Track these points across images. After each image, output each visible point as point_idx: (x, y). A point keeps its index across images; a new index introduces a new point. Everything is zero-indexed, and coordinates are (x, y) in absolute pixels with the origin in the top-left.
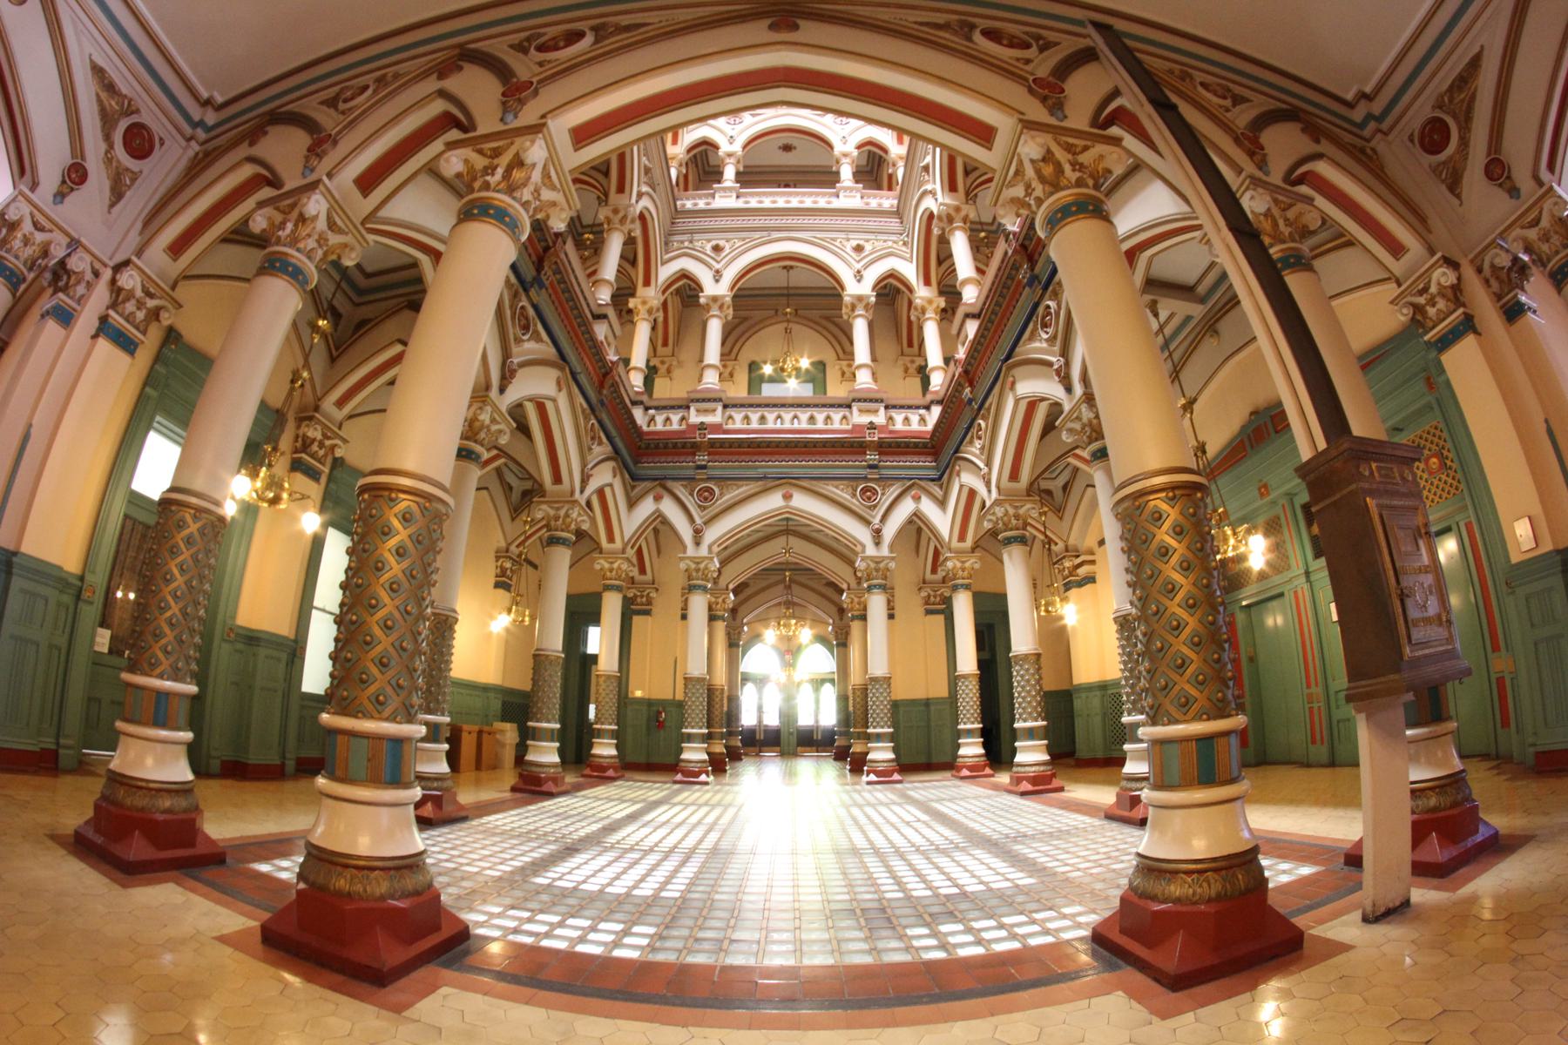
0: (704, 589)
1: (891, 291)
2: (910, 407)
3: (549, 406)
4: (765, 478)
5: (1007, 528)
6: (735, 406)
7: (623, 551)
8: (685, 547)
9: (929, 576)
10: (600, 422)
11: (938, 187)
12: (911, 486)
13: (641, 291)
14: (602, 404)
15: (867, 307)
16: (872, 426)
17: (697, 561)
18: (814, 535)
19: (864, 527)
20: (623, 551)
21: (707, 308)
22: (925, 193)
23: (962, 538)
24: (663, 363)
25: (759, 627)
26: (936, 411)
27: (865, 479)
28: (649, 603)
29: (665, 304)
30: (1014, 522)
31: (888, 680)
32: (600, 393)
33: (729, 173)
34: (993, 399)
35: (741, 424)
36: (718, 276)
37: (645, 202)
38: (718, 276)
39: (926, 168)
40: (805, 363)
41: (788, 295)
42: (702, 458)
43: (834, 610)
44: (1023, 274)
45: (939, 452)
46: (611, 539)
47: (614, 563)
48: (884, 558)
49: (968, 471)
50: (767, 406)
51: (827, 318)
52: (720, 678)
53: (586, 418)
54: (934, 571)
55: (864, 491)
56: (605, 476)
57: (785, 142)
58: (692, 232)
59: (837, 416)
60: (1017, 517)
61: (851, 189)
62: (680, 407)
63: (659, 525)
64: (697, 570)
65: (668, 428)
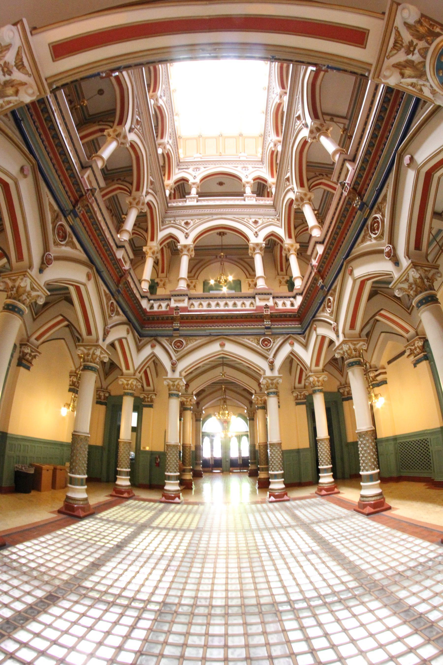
0: (178, 396)
1: (272, 245)
2: (285, 297)
3: (82, 288)
4: (210, 335)
5: (350, 357)
6: (194, 298)
7: (134, 374)
8: (167, 373)
9: (297, 385)
10: (118, 302)
11: (295, 185)
12: (289, 337)
13: (149, 243)
14: (118, 291)
15: (261, 249)
16: (267, 307)
17: (173, 380)
18: (237, 366)
19: (264, 361)
20: (134, 374)
21: (182, 250)
22: (288, 191)
23: (317, 364)
24: (161, 281)
25: (211, 411)
26: (299, 300)
27: (264, 335)
28: (152, 401)
29: (162, 249)
30: (354, 353)
31: (280, 444)
32: (118, 286)
33: (194, 191)
34: (338, 282)
35: (199, 307)
36: (187, 236)
37: (149, 198)
38: (187, 236)
39: (288, 179)
40: (231, 278)
41: (222, 249)
42: (177, 325)
43: (247, 402)
44: (357, 203)
45: (303, 320)
46: (128, 368)
47: (128, 380)
48: (275, 378)
49: (320, 326)
50: (211, 298)
51: (241, 259)
52: (190, 441)
53: (108, 299)
54: (300, 382)
55: (264, 341)
56: (120, 332)
57: (220, 181)
58: (175, 217)
59: (248, 302)
60: (355, 350)
61: (251, 197)
62: (166, 299)
63: (155, 361)
64: (174, 385)
65: (160, 310)
